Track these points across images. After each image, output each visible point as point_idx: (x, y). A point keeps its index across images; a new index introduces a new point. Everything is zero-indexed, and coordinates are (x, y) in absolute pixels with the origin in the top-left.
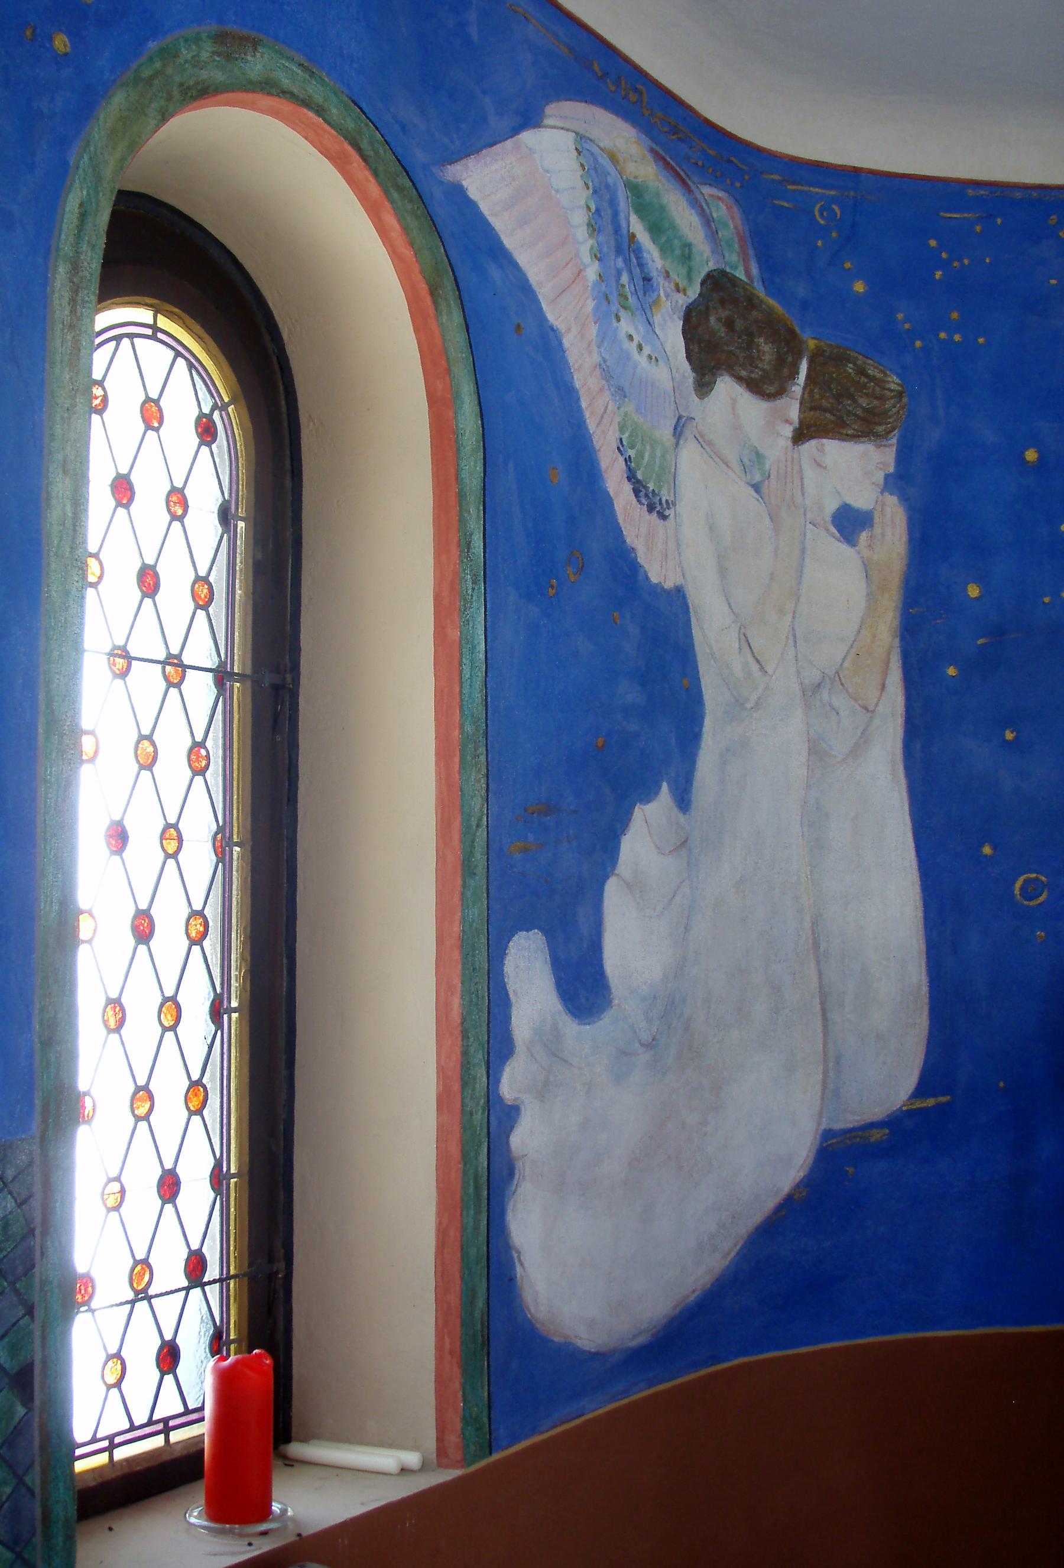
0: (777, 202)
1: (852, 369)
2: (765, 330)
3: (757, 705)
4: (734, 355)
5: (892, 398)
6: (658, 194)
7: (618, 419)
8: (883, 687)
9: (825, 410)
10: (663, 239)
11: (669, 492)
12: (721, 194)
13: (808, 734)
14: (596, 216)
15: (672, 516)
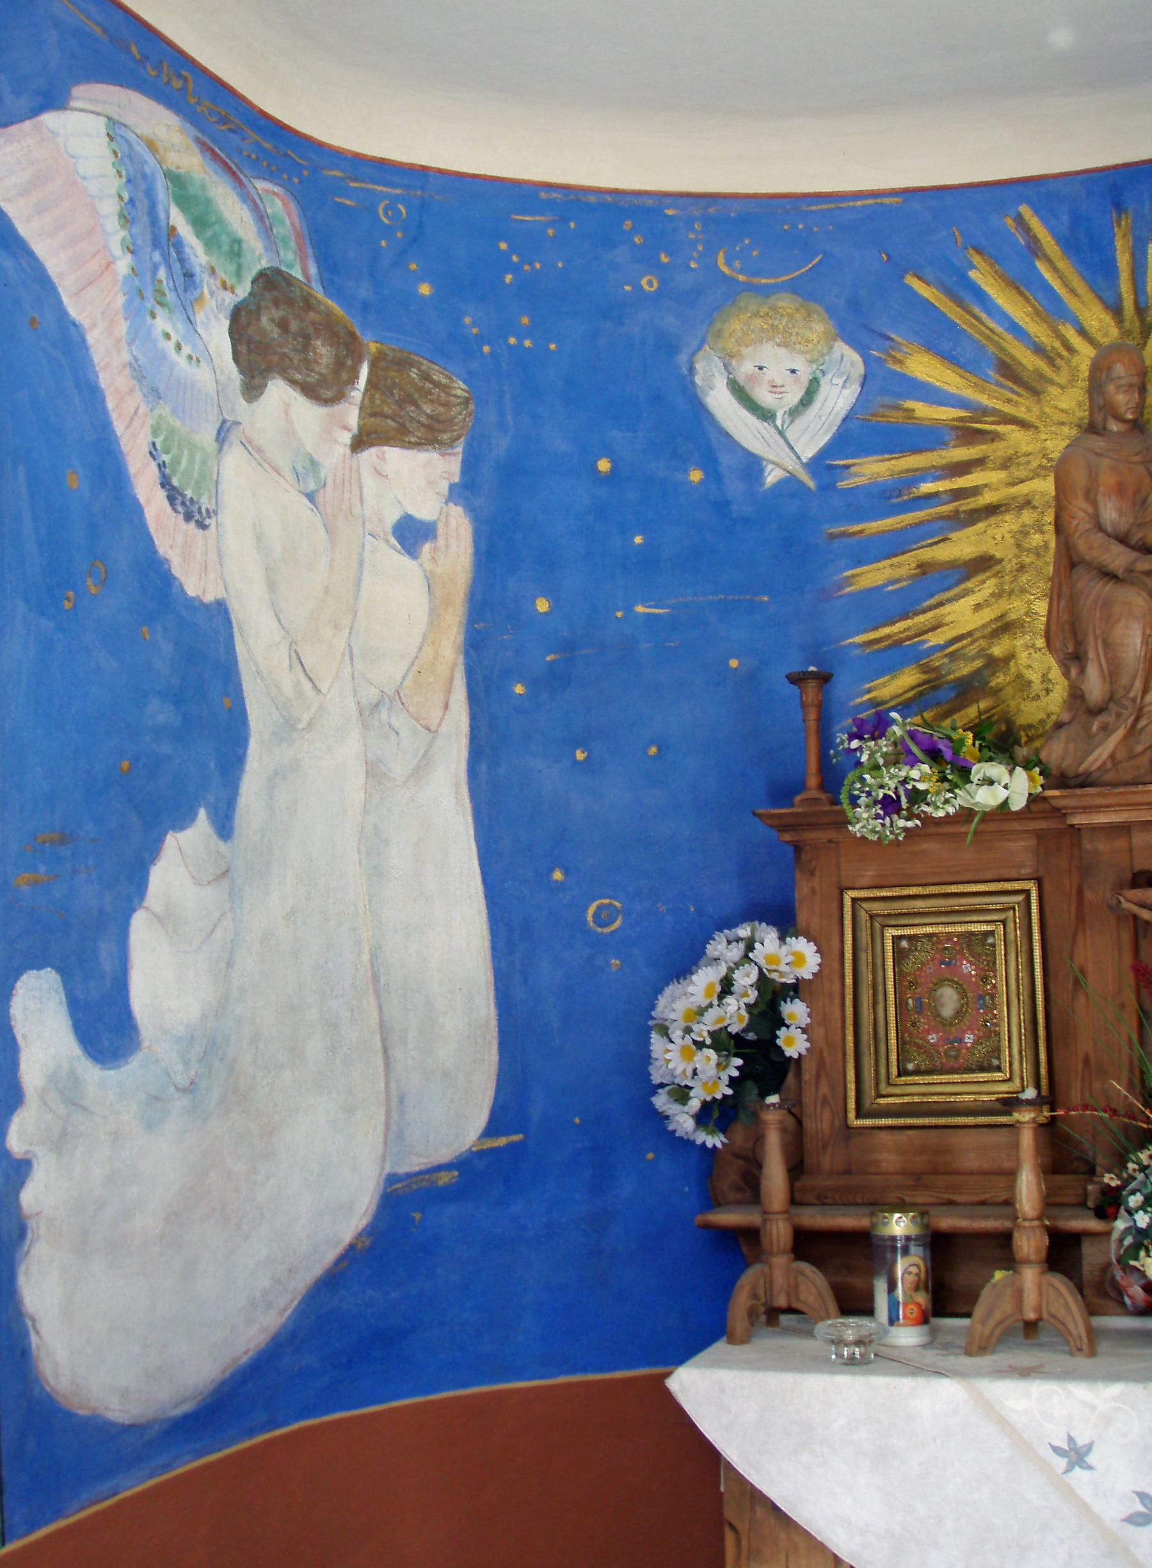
0: (338, 200)
1: (416, 374)
2: (323, 332)
3: (310, 725)
4: (288, 357)
5: (458, 404)
6: (203, 187)
7: (150, 421)
8: (446, 706)
9: (387, 417)
10: (209, 234)
11: (210, 499)
12: (277, 189)
13: (366, 756)
14: (129, 207)
15: (213, 526)
